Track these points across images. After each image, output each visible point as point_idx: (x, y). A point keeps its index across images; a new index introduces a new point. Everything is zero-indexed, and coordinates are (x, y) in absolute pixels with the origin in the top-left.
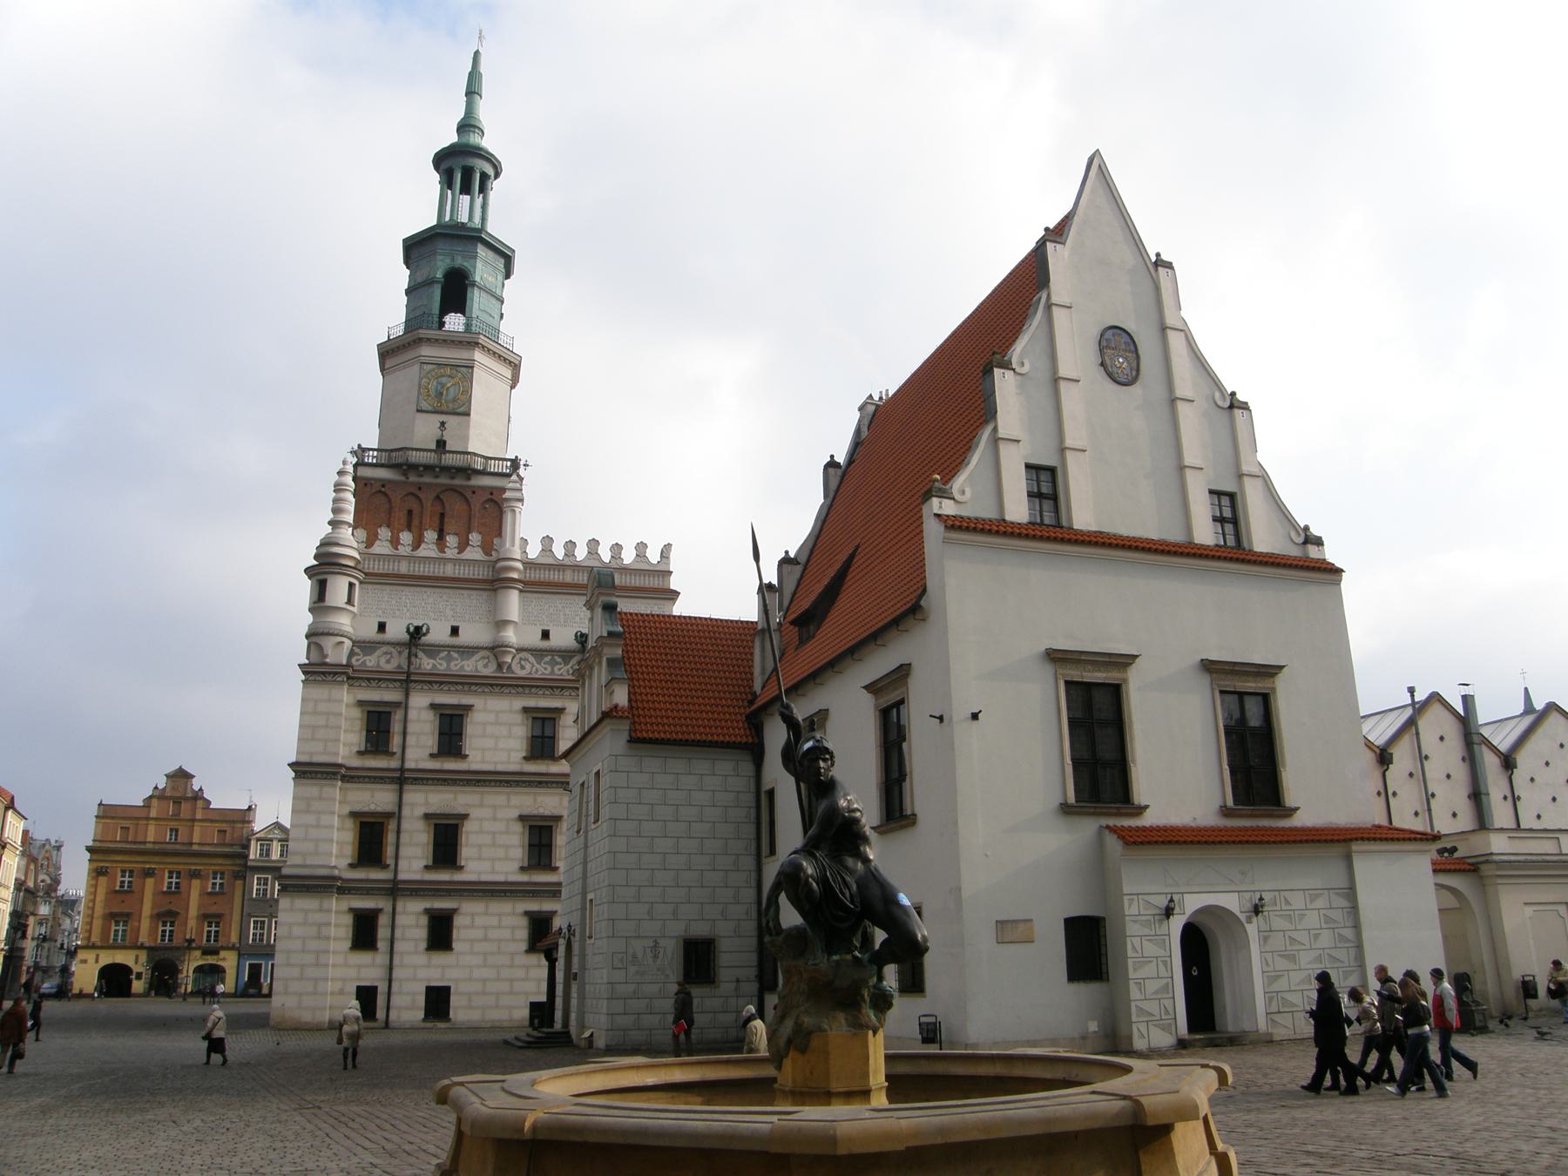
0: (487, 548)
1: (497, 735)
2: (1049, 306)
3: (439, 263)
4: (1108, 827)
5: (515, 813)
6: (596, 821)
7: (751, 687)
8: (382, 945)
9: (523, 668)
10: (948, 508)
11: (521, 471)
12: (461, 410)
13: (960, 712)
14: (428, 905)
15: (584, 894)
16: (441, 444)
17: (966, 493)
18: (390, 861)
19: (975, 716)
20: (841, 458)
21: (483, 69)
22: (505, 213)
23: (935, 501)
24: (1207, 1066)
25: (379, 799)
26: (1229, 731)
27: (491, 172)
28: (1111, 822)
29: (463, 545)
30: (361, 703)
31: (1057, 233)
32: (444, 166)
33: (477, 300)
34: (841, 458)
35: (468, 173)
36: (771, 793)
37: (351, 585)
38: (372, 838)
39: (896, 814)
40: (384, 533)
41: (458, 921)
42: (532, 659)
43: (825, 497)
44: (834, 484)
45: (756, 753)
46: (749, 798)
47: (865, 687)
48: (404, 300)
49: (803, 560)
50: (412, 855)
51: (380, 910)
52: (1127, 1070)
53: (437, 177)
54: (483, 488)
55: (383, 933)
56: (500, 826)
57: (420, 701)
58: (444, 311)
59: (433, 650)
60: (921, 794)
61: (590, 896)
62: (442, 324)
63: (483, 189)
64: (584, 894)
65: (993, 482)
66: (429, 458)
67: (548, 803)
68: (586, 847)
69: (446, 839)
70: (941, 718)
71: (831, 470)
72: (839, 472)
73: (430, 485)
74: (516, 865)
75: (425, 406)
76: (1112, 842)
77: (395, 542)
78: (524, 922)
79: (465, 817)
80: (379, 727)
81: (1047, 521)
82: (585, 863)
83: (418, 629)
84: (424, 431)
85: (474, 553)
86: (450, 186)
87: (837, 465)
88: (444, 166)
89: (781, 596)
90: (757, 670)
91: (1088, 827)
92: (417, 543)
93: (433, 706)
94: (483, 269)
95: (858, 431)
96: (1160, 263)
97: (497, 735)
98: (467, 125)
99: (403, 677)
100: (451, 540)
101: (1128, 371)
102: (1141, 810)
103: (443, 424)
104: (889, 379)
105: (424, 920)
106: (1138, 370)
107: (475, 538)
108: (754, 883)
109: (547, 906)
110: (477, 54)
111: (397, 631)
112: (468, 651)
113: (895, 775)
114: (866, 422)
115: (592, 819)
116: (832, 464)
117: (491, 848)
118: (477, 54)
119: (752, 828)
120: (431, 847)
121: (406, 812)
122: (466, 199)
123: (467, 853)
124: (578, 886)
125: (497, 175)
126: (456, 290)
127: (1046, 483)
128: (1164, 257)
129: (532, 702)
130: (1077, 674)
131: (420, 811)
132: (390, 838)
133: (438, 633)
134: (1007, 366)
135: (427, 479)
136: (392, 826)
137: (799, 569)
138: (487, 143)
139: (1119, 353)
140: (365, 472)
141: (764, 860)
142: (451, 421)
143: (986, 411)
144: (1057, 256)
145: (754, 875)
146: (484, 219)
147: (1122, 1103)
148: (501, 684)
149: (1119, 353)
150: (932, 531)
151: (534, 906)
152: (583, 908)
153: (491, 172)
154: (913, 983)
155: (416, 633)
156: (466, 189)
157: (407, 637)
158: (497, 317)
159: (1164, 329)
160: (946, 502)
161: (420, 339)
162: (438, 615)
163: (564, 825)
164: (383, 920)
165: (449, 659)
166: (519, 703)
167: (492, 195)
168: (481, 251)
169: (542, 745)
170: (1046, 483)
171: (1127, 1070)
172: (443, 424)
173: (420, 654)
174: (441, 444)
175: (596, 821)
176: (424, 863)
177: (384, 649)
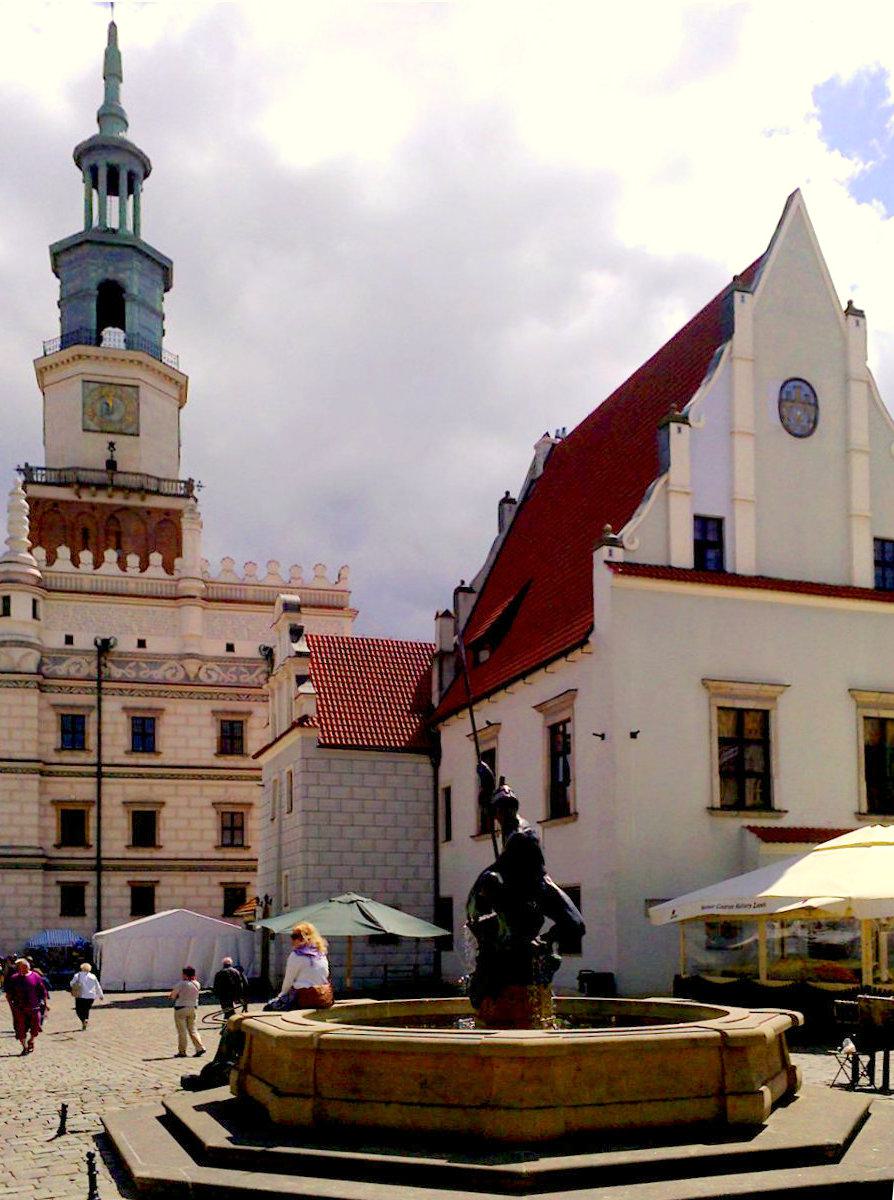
0: (169, 567)
1: (189, 732)
2: (731, 359)
3: (93, 275)
4: (749, 827)
5: (208, 802)
6: (290, 811)
7: (430, 701)
8: (90, 911)
9: (210, 677)
10: (619, 555)
11: (195, 492)
12: (130, 431)
13: (619, 736)
14: (131, 879)
15: (280, 872)
16: (111, 465)
17: (639, 537)
18: (93, 841)
19: (634, 735)
20: (516, 494)
21: (122, 45)
22: (160, 216)
23: (605, 549)
24: (785, 1014)
25: (83, 789)
26: (868, 748)
27: (140, 172)
28: (753, 822)
29: (144, 565)
30: (214, 713)
31: (746, 280)
32: (86, 162)
33: (132, 312)
34: (516, 494)
35: (113, 173)
36: (448, 791)
37: (35, 602)
38: (73, 824)
39: (560, 807)
40: (64, 552)
41: (159, 891)
42: (217, 669)
43: (500, 531)
44: (509, 519)
45: (427, 745)
46: (428, 795)
47: (194, 1107)
48: (57, 313)
49: (478, 588)
50: (116, 837)
51: (86, 883)
52: (727, 1013)
53: (79, 174)
54: (158, 510)
55: (90, 901)
56: (195, 813)
57: (112, 706)
58: (101, 327)
59: (123, 660)
60: (581, 794)
61: (285, 873)
62: (99, 340)
63: (131, 190)
64: (280, 872)
65: (661, 527)
66: (103, 477)
67: (239, 792)
68: (280, 832)
69: (144, 826)
70: (603, 736)
71: (506, 506)
72: (515, 508)
73: (104, 505)
74: (210, 846)
75: (93, 426)
76: (751, 838)
77: (75, 561)
78: (220, 891)
79: (163, 804)
80: (73, 731)
81: (888, 586)
82: (280, 847)
83: (106, 642)
84: (91, 452)
85: (156, 569)
86: (95, 185)
87: (513, 501)
88: (86, 162)
89: (457, 622)
90: (435, 687)
91: (735, 823)
92: (97, 564)
93: (125, 709)
94: (134, 280)
95: (533, 468)
96: (851, 310)
97: (189, 732)
98: (110, 114)
99: (105, 685)
100: (133, 560)
101: (805, 423)
102: (782, 812)
103: (112, 445)
104: (571, 416)
105: (128, 891)
106: (815, 422)
107: (156, 558)
108: (431, 863)
109: (240, 878)
110: (113, 26)
111: (85, 641)
112: (156, 660)
113: (160, 1189)
114: (541, 460)
115: (285, 810)
116: (507, 500)
117: (190, 827)
118: (113, 26)
119: (429, 820)
120: (131, 832)
121: (105, 801)
122: (113, 202)
123: (165, 832)
124: (273, 865)
125: (146, 175)
126: (111, 305)
127: (709, 534)
128: (857, 305)
129: (219, 705)
130: (65, 712)
131: (118, 800)
132: (92, 823)
133: (126, 644)
134: (685, 420)
135: (101, 498)
136: (93, 812)
137: (472, 599)
138: (134, 136)
139: (798, 407)
140: (37, 491)
141: (441, 845)
142: (121, 441)
143: (654, 464)
144: (744, 309)
145: (432, 857)
146: (136, 226)
147: (718, 1034)
148: (189, 688)
149: (798, 407)
150: (602, 576)
151: (228, 878)
152: (279, 883)
153: (140, 172)
154: (571, 936)
155: (104, 647)
156: (113, 190)
157: (95, 648)
158: (159, 333)
159: (847, 379)
160: (615, 549)
161: (80, 357)
162: (125, 624)
163: (256, 813)
164: (90, 891)
165: (238, 673)
166: (207, 707)
167: (144, 198)
168: (137, 263)
169: (231, 738)
170: (709, 534)
171: (727, 1013)
172: (112, 445)
173: (109, 664)
174: (111, 465)
175: (290, 811)
176: (126, 843)
177: (74, 659)
